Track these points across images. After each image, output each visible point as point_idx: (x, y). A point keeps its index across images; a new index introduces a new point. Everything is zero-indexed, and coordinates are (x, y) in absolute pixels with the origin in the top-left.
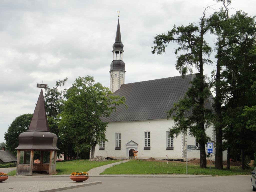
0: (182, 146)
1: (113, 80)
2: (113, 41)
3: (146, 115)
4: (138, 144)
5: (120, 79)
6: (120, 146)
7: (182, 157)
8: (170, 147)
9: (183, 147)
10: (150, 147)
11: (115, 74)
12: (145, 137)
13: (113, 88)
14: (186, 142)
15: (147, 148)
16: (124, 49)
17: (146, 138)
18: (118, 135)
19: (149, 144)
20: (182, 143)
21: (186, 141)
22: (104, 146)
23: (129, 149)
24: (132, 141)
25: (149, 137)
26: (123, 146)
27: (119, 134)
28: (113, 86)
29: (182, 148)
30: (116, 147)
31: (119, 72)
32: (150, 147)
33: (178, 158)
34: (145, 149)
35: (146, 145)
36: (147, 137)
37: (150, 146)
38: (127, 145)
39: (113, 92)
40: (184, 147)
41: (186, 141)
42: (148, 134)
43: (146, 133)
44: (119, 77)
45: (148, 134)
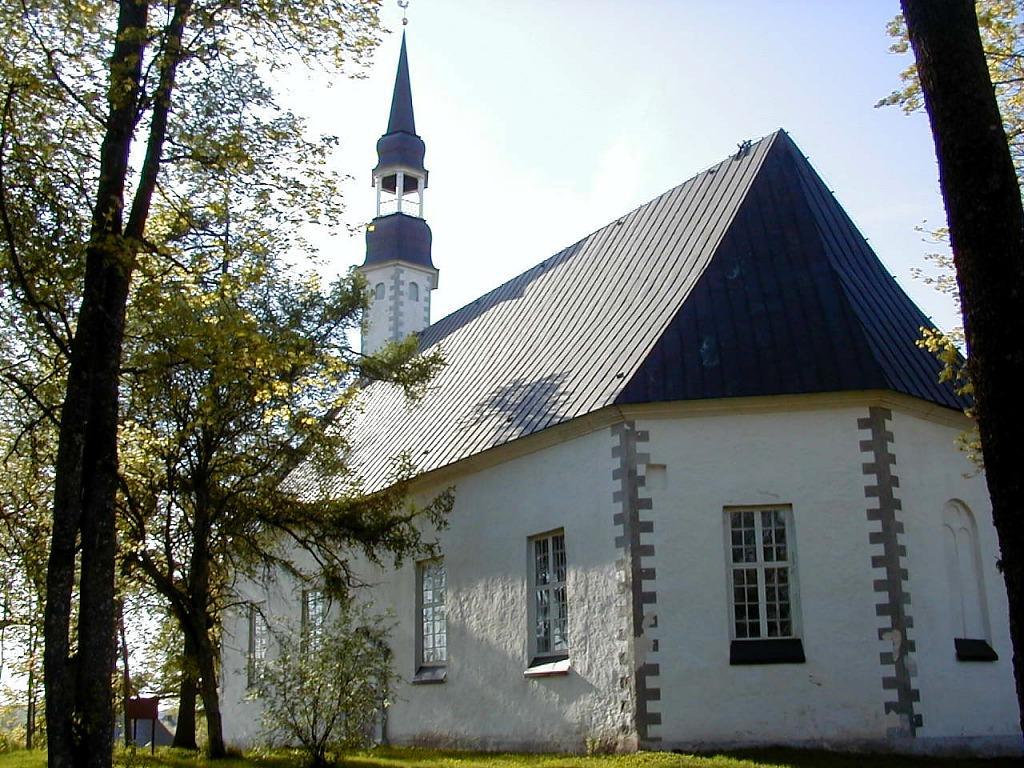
2: (380, 125)
5: (399, 304)
7: (889, 707)
14: (647, 608)
16: (428, 162)
21: (651, 598)
31: (391, 271)
41: (651, 598)
44: (391, 298)
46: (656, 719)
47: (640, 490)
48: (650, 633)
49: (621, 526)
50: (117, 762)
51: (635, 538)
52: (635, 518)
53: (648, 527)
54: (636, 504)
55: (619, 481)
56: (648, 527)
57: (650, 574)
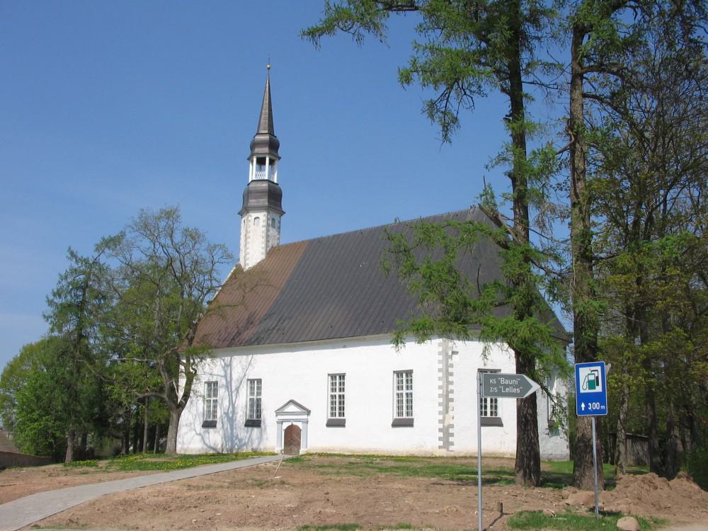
0: (440, 413)
1: (248, 235)
3: (381, 324)
4: (308, 412)
6: (259, 416)
7: (440, 447)
8: (405, 416)
9: (441, 417)
10: (413, 419)
11: (253, 218)
12: (330, 390)
13: (248, 256)
14: (450, 404)
15: (336, 422)
17: (400, 392)
18: (256, 384)
19: (342, 408)
20: (440, 404)
21: (452, 400)
22: (342, 414)
23: (285, 425)
24: (292, 402)
25: (342, 390)
26: (269, 417)
27: (338, 377)
28: (248, 251)
29: (440, 421)
30: (396, 416)
32: (345, 420)
33: (427, 450)
34: (331, 424)
35: (332, 414)
36: (404, 387)
37: (412, 415)
38: (279, 412)
39: (247, 268)
40: (444, 418)
41: (452, 400)
42: (338, 380)
43: (333, 377)
45: (338, 380)
46: (452, 444)
47: (450, 360)
48: (451, 413)
49: (251, 451)
50: (686, 407)
51: (447, 378)
52: (447, 370)
53: (452, 374)
54: (448, 366)
55: (441, 356)
56: (452, 374)
57: (452, 392)
